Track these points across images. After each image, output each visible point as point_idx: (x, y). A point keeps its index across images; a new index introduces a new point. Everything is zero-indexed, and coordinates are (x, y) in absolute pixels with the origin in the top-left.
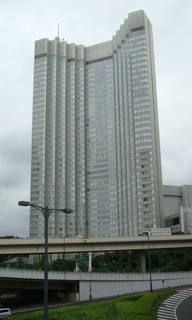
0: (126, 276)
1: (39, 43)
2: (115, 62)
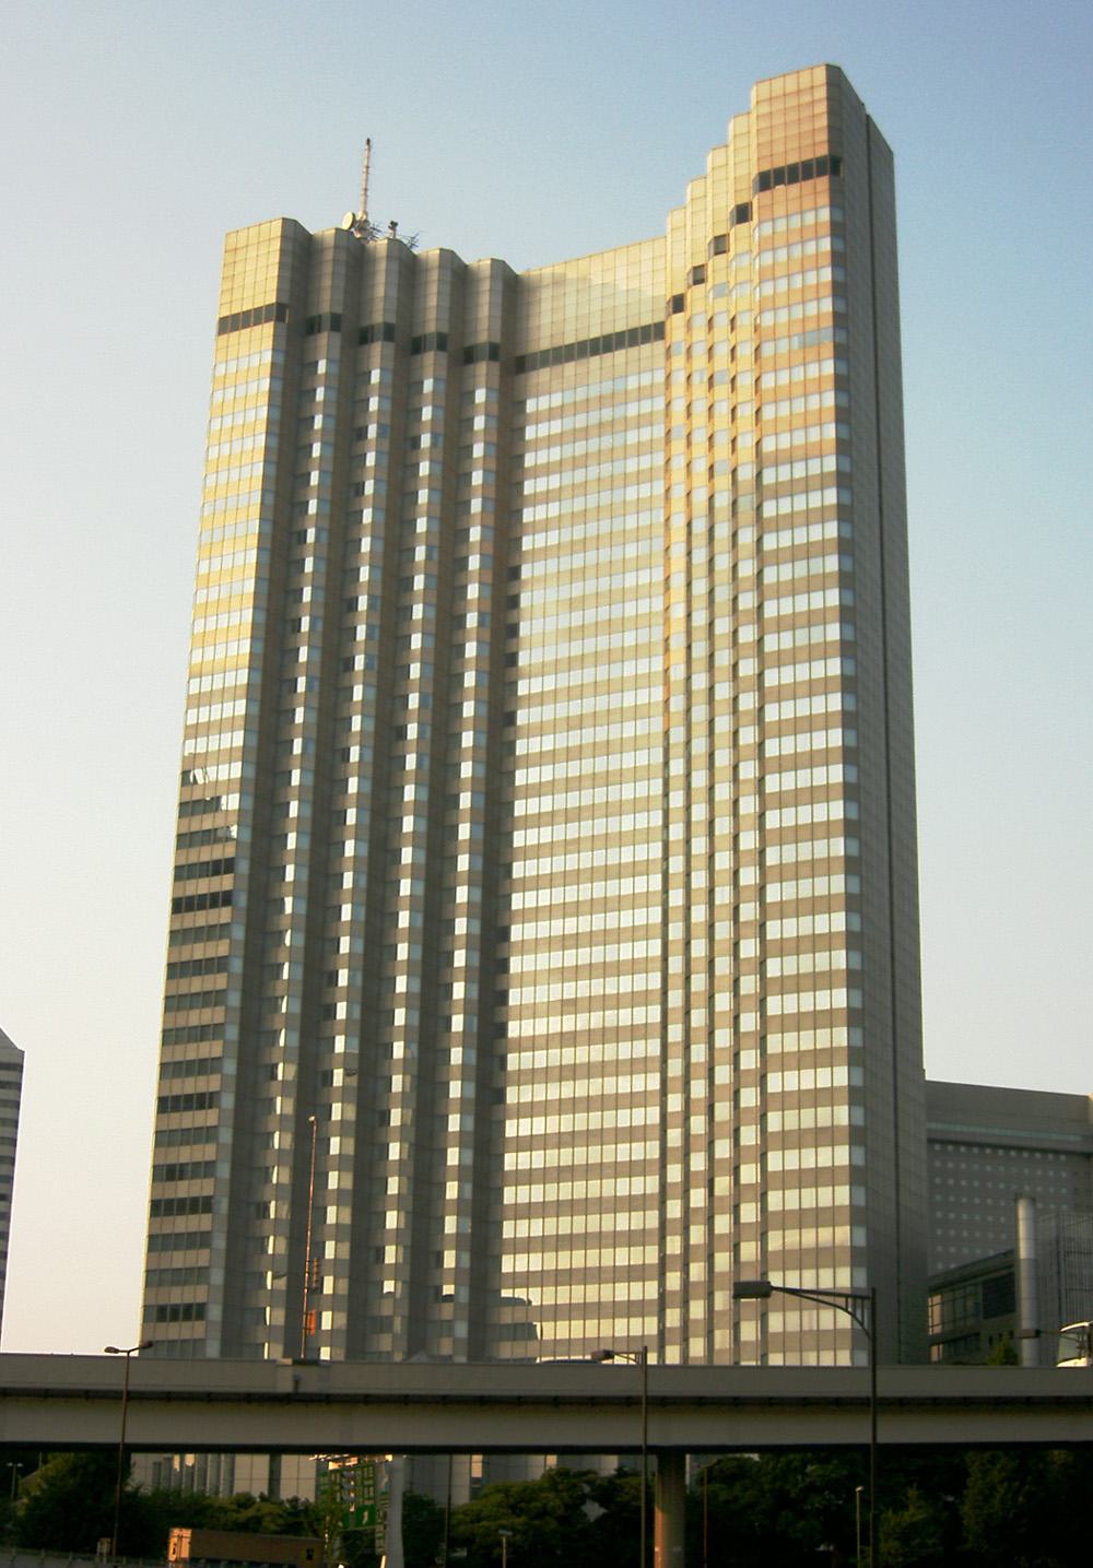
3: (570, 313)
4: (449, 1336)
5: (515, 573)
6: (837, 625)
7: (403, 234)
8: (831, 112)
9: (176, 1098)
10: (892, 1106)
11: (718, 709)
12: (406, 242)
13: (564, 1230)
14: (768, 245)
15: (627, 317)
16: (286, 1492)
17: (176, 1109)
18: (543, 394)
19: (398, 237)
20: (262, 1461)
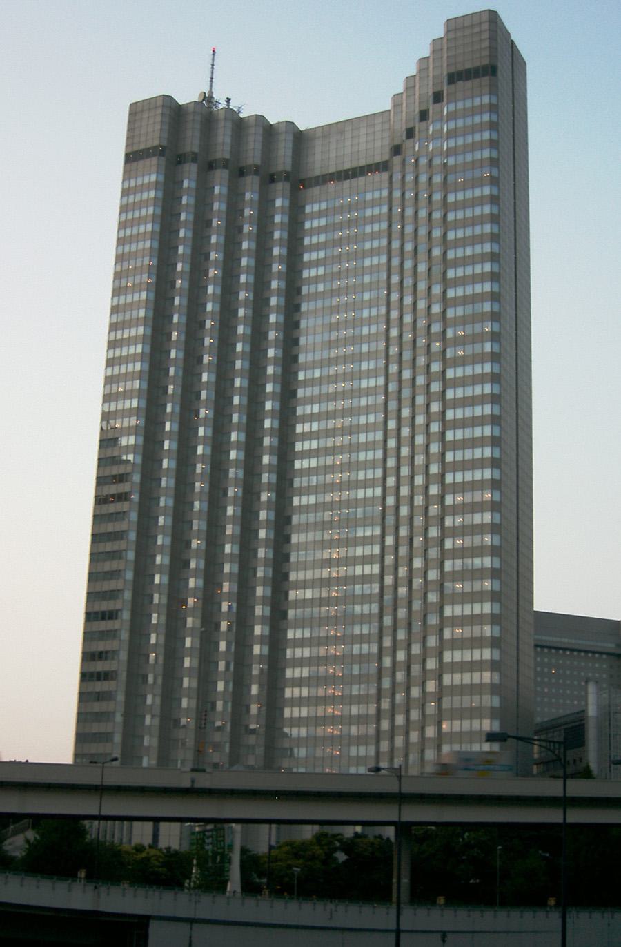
1: (142, 111)
2: (397, 184)
3: (333, 154)
4: (253, 754)
5: (297, 308)
9: (96, 613)
10: (515, 626)
11: (419, 351)
12: (235, 110)
14: (453, 116)
15: (366, 157)
17: (96, 619)
18: (316, 202)
19: (231, 107)
20: (149, 826)
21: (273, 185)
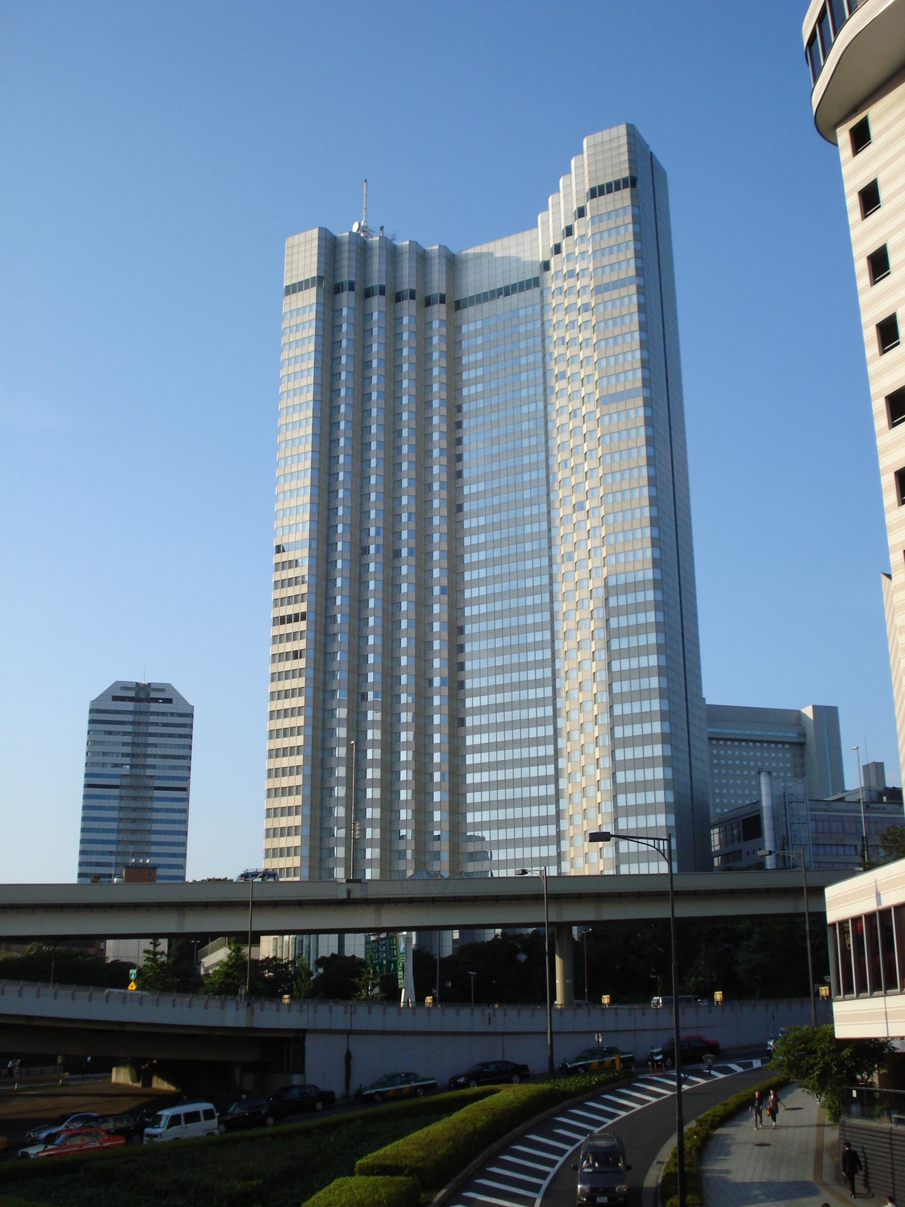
0: (483, 1015)
6: (654, 634)
7: (388, 233)
8: (630, 151)
12: (389, 237)
13: (502, 817)
16: (348, 953)
21: (459, 312)
